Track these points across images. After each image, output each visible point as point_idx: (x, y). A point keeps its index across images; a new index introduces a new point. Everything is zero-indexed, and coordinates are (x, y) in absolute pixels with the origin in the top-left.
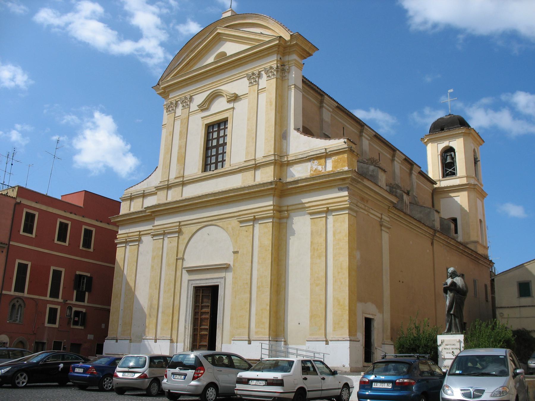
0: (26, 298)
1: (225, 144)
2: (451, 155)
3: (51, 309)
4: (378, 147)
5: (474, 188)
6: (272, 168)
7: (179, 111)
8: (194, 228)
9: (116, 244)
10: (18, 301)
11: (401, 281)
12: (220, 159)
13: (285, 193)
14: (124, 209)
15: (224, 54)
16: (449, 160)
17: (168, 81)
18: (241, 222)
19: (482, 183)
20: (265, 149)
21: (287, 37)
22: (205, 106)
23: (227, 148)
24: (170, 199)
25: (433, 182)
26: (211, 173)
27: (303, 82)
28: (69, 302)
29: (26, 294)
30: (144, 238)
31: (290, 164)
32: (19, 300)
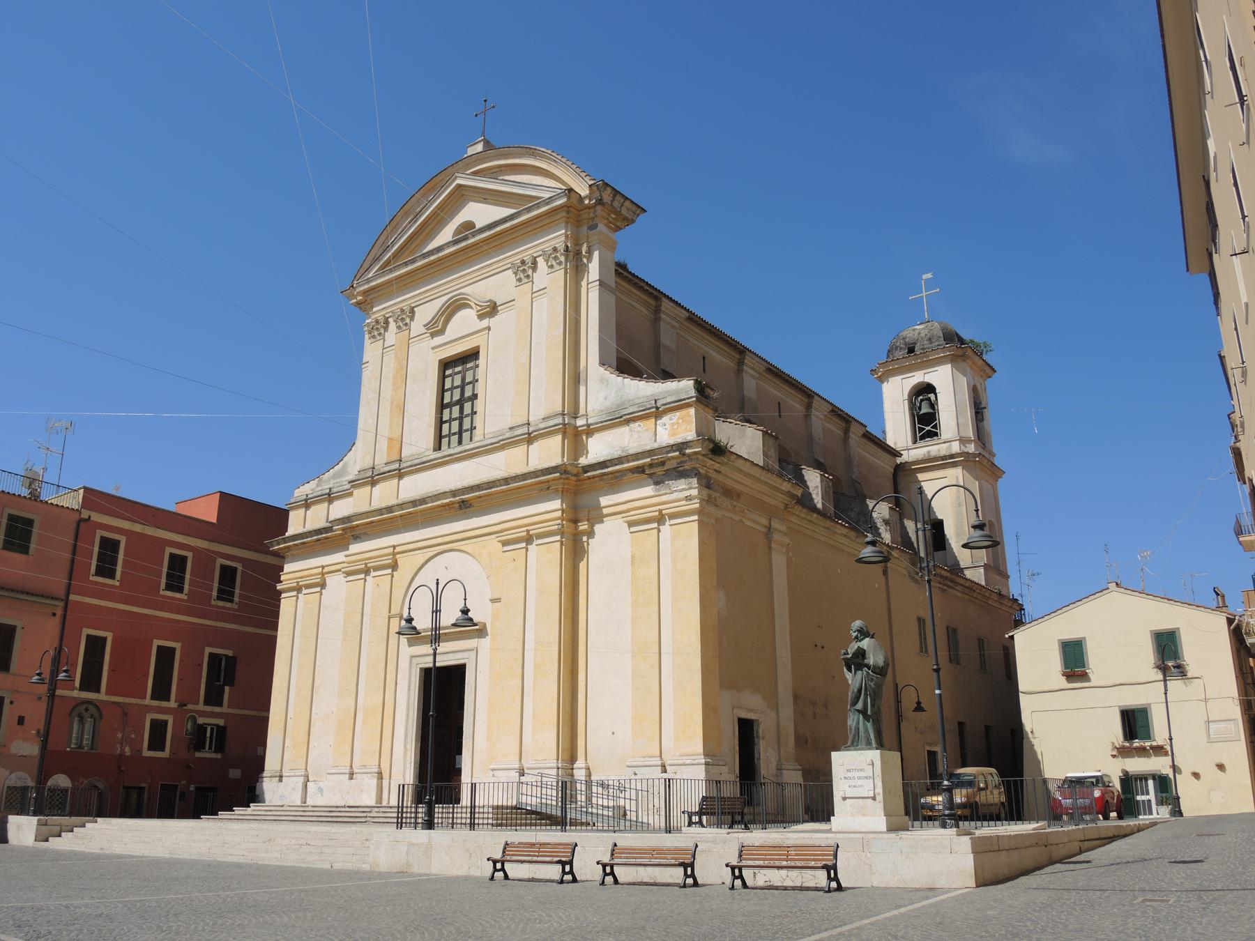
0: (102, 702)
1: (475, 396)
2: (929, 399)
3: (153, 722)
4: (776, 391)
5: (981, 462)
6: (558, 438)
7: (391, 335)
8: (420, 557)
9: (280, 593)
10: (87, 710)
11: (819, 645)
12: (467, 425)
13: (579, 490)
14: (296, 524)
15: (469, 225)
16: (925, 409)
17: (369, 281)
18: (505, 543)
19: (995, 450)
20: (546, 401)
21: (583, 191)
22: (436, 328)
23: (479, 404)
24: (376, 504)
25: (895, 453)
26: (460, 449)
27: (617, 273)
28: (189, 707)
29: (102, 696)
30: (330, 580)
31: (590, 431)
32: (90, 707)
